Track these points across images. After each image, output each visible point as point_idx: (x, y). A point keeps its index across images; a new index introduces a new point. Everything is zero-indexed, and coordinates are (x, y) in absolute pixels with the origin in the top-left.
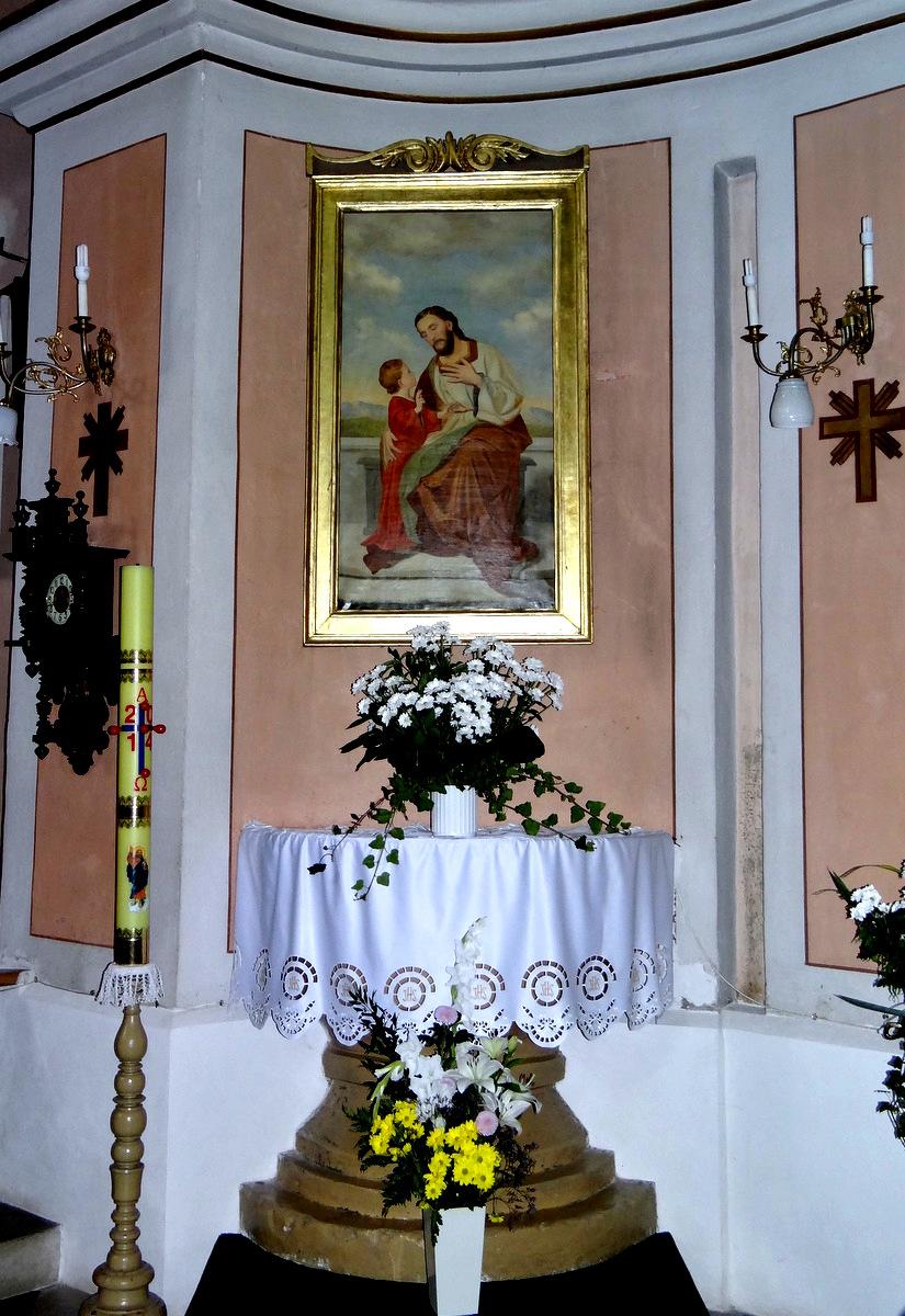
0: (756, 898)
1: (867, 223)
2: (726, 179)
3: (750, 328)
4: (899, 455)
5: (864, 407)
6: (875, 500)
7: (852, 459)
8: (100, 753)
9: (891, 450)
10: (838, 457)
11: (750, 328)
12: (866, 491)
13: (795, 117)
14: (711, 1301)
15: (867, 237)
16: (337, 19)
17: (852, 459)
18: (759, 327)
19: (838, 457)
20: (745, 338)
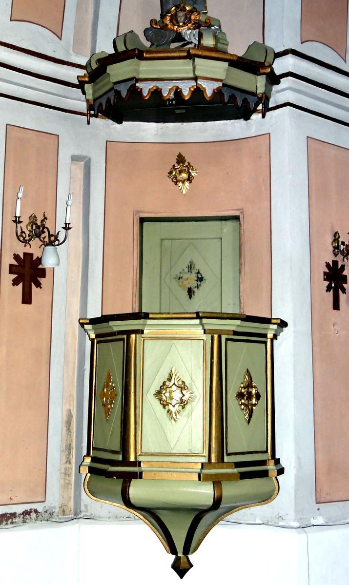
0: (235, 410)
1: (22, 189)
2: (82, 161)
3: (66, 224)
4: (345, 293)
5: (27, 266)
6: (339, 310)
7: (21, 285)
8: (38, 285)
9: (344, 291)
10: (15, 283)
11: (66, 224)
12: (336, 306)
13: (58, 136)
14: (133, 480)
15: (20, 195)
16: (316, 81)
17: (21, 285)
18: (69, 224)
19: (15, 283)
20: (63, 228)
